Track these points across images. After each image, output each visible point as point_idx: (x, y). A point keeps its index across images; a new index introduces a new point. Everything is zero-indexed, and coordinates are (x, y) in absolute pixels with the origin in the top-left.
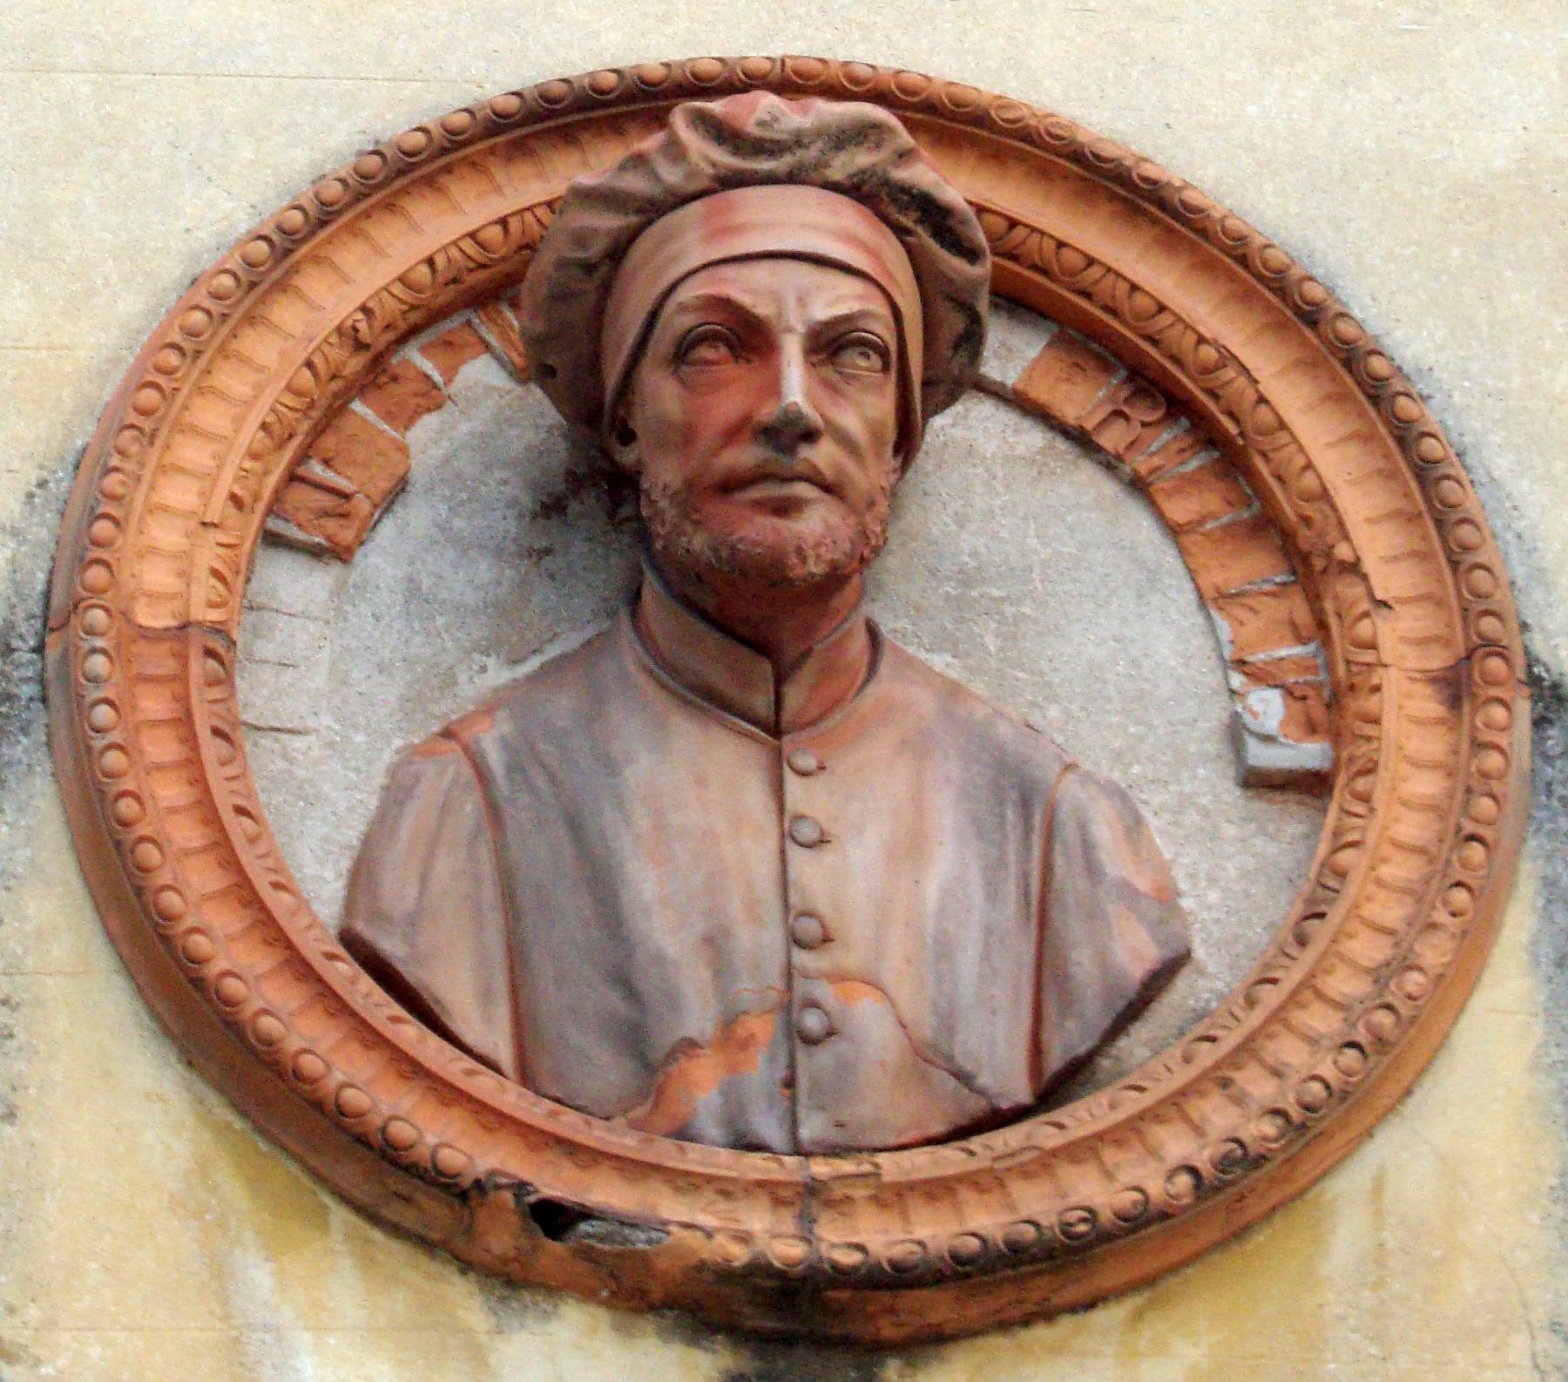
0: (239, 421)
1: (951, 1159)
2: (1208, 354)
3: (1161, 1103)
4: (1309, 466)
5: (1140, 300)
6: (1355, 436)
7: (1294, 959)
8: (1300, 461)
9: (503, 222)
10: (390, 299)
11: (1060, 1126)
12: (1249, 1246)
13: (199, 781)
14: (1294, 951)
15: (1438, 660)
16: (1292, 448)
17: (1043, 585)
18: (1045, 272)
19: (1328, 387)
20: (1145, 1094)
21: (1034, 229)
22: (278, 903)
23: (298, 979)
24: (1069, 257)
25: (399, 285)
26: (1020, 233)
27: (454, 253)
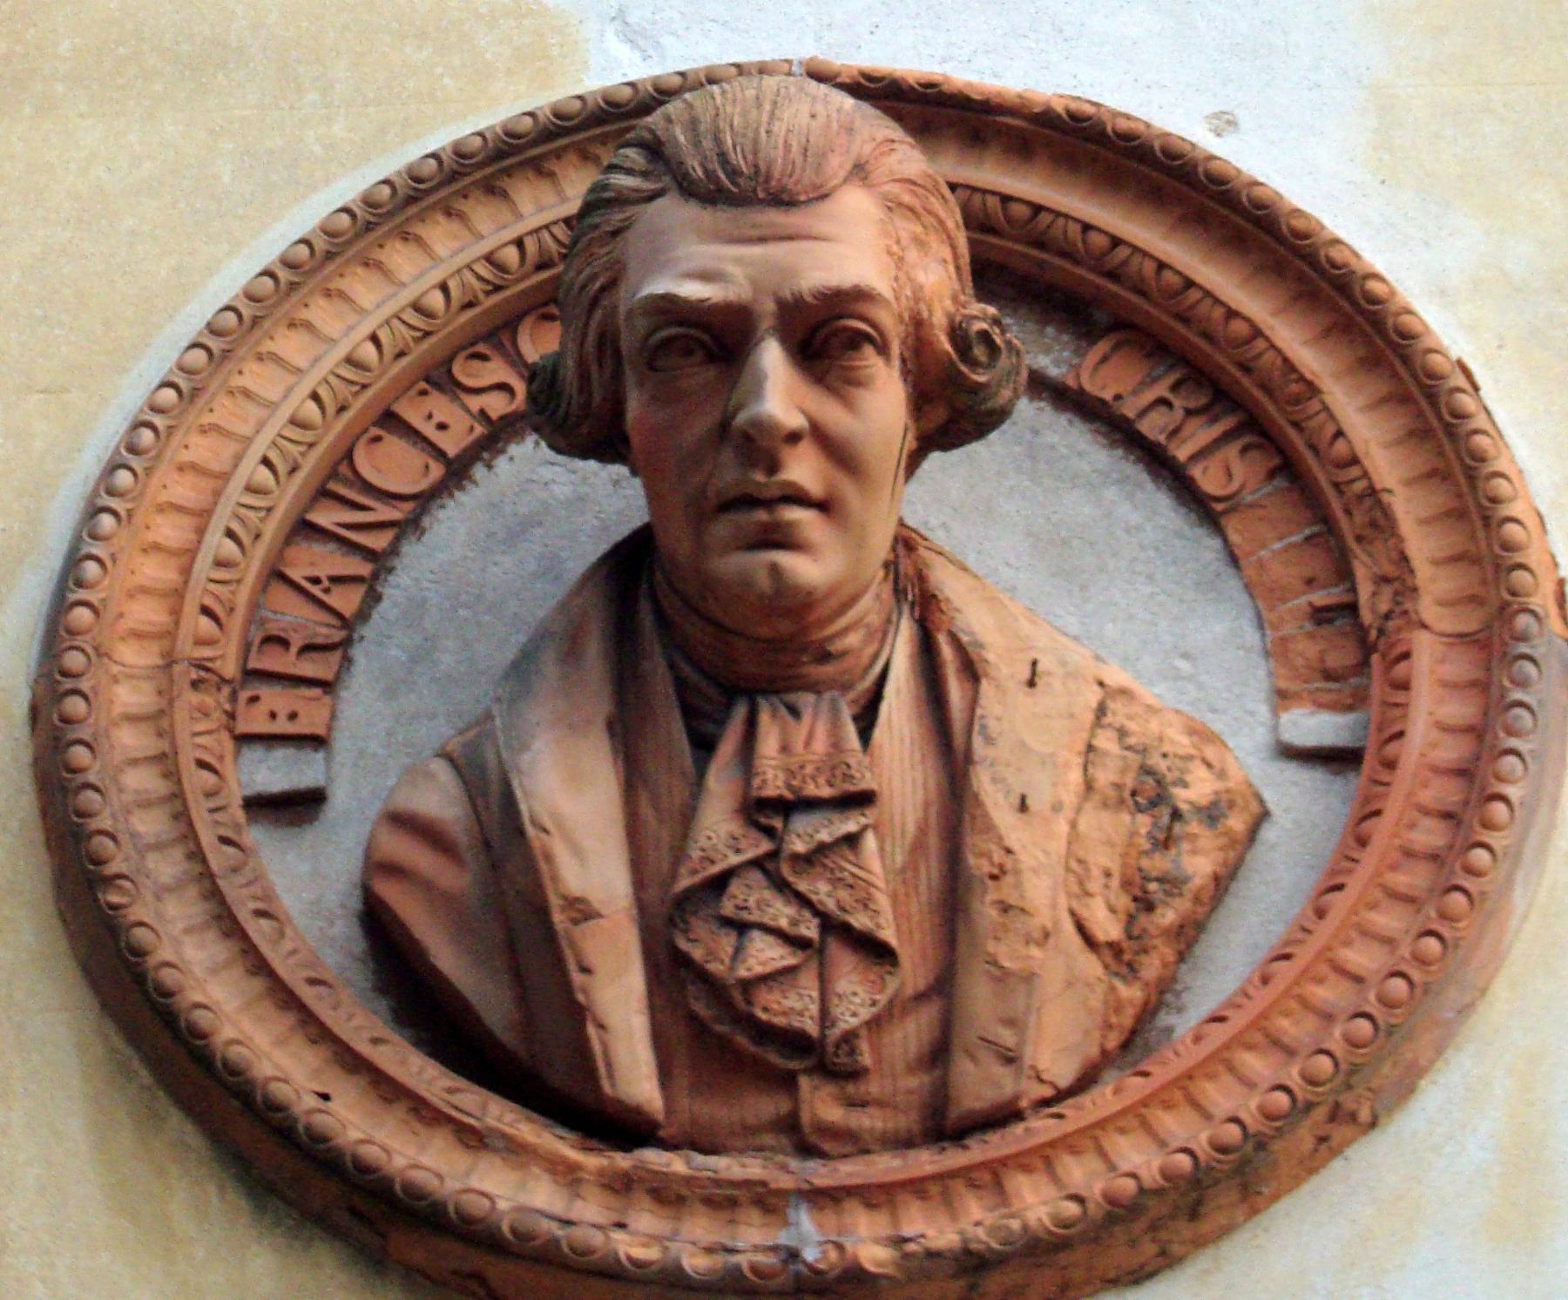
0: (238, 459)
1: (926, 1161)
2: (1238, 327)
3: (1081, 1132)
4: (1340, 433)
5: (1168, 276)
6: (1385, 400)
7: (1387, 784)
8: (1330, 429)
9: (519, 243)
10: (403, 328)
11: (1146, 1074)
12: (1201, 532)
13: (182, 816)
14: (1385, 777)
15: (1469, 621)
16: (1323, 416)
17: (1080, 616)
18: (1142, 293)
19: (1362, 352)
20: (1150, 1079)
21: (1058, 214)
22: (259, 930)
23: (282, 1008)
24: (1097, 240)
25: (410, 311)
26: (1045, 218)
27: (469, 277)
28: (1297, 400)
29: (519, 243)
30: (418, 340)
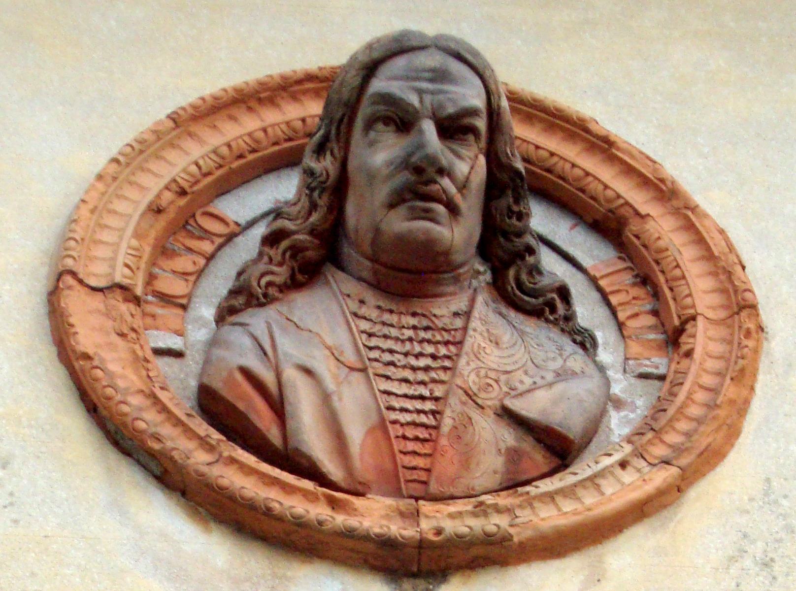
4: (690, 295)
5: (677, 272)
8: (687, 292)
28: (676, 279)
29: (265, 130)
30: (217, 168)
